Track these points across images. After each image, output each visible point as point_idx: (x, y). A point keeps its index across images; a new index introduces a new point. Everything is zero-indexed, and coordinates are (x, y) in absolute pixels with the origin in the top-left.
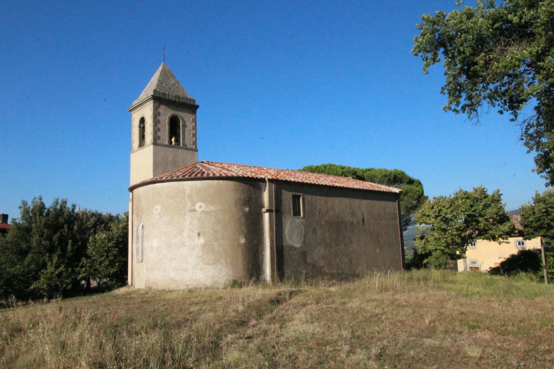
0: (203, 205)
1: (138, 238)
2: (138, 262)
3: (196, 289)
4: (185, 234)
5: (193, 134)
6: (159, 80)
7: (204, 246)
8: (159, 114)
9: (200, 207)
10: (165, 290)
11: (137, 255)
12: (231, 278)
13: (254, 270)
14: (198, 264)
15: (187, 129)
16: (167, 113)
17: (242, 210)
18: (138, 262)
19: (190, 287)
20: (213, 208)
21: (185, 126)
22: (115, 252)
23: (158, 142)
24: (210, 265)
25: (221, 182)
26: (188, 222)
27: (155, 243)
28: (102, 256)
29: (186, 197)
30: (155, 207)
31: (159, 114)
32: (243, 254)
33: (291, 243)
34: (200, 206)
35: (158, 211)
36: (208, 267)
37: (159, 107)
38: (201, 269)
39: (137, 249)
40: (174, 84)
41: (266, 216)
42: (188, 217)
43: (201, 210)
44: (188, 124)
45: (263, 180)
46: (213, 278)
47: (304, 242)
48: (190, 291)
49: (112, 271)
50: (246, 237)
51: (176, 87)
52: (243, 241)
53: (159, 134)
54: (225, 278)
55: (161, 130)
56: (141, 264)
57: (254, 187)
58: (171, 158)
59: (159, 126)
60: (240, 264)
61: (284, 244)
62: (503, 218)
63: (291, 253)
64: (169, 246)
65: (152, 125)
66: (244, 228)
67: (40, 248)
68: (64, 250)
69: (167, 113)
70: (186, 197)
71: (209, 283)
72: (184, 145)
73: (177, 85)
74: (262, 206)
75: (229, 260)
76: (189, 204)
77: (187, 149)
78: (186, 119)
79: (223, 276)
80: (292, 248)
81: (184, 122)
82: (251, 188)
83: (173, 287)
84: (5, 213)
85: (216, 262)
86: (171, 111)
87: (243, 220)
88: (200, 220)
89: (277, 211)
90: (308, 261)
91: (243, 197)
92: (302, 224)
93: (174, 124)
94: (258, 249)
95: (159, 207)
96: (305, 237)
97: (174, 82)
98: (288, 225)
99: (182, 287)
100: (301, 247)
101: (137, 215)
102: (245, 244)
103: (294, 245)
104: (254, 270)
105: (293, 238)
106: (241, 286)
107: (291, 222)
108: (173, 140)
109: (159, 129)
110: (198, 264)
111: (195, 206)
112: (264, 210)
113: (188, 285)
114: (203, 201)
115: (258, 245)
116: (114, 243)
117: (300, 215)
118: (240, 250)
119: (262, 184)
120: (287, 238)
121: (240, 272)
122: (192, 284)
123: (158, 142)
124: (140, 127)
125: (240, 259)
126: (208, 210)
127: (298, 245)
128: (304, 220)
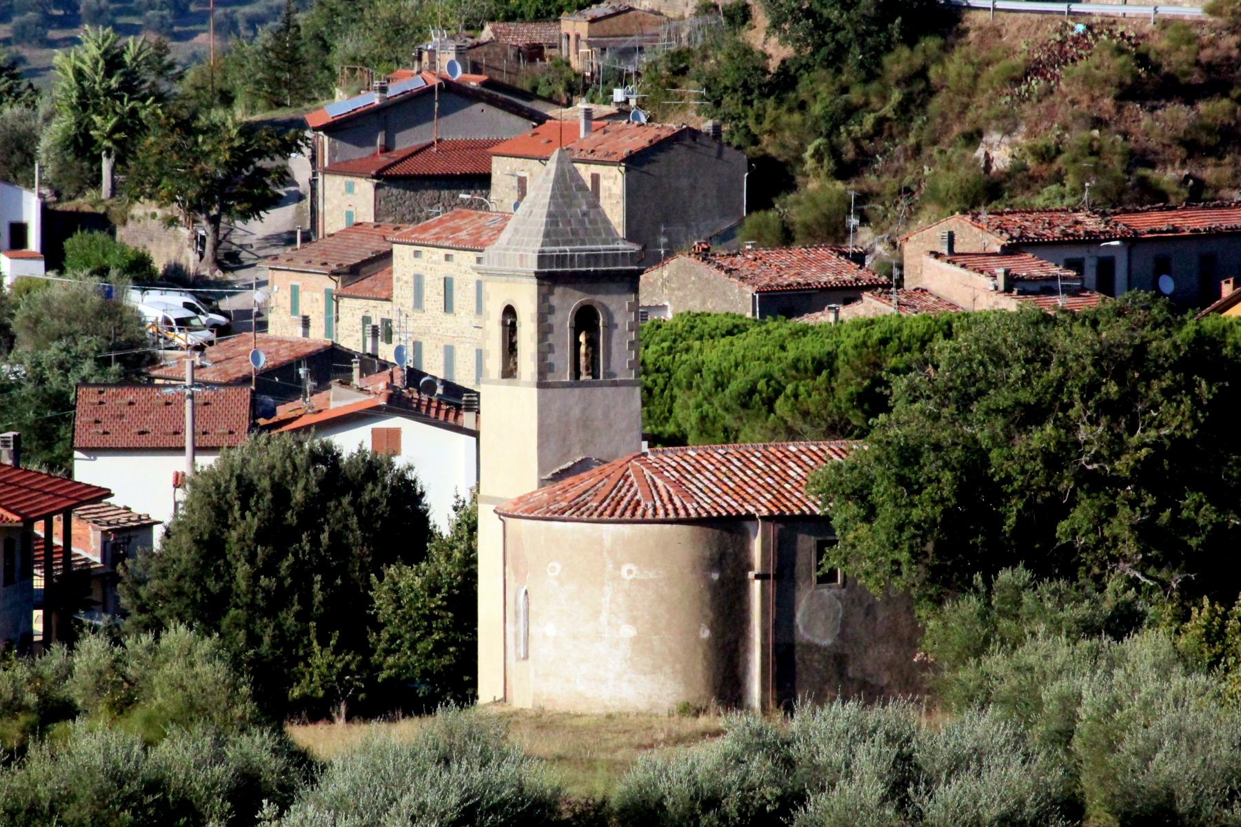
0: (634, 568)
1: (516, 614)
2: (518, 659)
3: (620, 714)
4: (604, 618)
5: (631, 343)
6: (550, 215)
7: (636, 641)
8: (551, 310)
9: (630, 572)
10: (568, 714)
11: (517, 646)
12: (682, 699)
13: (728, 689)
14: (625, 672)
15: (616, 333)
16: (568, 302)
17: (706, 578)
18: (518, 659)
19: (611, 711)
20: (651, 575)
21: (610, 326)
22: (447, 621)
23: (550, 379)
24: (645, 674)
25: (668, 526)
26: (608, 598)
27: (550, 630)
28: (416, 629)
29: (605, 554)
30: (550, 565)
31: (551, 310)
32: (705, 656)
33: (808, 637)
34: (628, 571)
35: (556, 573)
36: (642, 678)
37: (551, 293)
38: (630, 681)
39: (516, 635)
40: (584, 214)
41: (757, 584)
42: (608, 591)
43: (631, 577)
44: (618, 319)
45: (750, 517)
46: (650, 697)
47: (842, 636)
48: (610, 717)
49: (437, 663)
50: (712, 628)
51: (591, 222)
52: (706, 634)
53: (551, 358)
54: (671, 699)
55: (556, 349)
56: (524, 663)
57: (731, 532)
58: (576, 411)
59: (551, 339)
60: (699, 675)
61: (798, 639)
62: (279, 743)
63: (807, 657)
64: (575, 637)
65: (535, 318)
66: (708, 612)
67: (254, 594)
68: (307, 599)
69: (568, 302)
70: (605, 554)
71: (643, 706)
72: (609, 374)
73: (592, 212)
74: (750, 567)
75: (678, 667)
76: (610, 566)
77: (616, 384)
78: (612, 307)
79: (668, 695)
80: (811, 647)
81: (609, 316)
82: (725, 534)
83: (581, 709)
84: (170, 481)
85: (656, 669)
86: (578, 294)
87: (707, 596)
88: (629, 595)
89: (782, 576)
90: (850, 675)
91: (708, 553)
92: (839, 598)
93: (586, 319)
94: (736, 650)
95: (558, 566)
96: (844, 624)
97: (584, 208)
98: (803, 602)
99: (598, 711)
100: (833, 645)
101: (516, 572)
102: (710, 639)
103: (817, 641)
104: (728, 689)
105: (815, 620)
106: (697, 713)
107: (812, 596)
108: (582, 338)
109: (551, 328)
110: (625, 672)
111: (620, 569)
112: (751, 575)
113: (606, 707)
114: (634, 562)
115: (737, 642)
116: (443, 599)
117: (836, 580)
118: (700, 650)
119: (748, 524)
120: (801, 628)
121: (698, 688)
122: (614, 707)
123: (550, 379)
124: (504, 324)
125: (699, 668)
126: (642, 577)
127: (827, 642)
128: (844, 591)
